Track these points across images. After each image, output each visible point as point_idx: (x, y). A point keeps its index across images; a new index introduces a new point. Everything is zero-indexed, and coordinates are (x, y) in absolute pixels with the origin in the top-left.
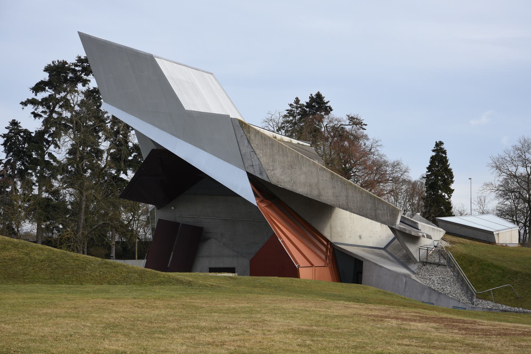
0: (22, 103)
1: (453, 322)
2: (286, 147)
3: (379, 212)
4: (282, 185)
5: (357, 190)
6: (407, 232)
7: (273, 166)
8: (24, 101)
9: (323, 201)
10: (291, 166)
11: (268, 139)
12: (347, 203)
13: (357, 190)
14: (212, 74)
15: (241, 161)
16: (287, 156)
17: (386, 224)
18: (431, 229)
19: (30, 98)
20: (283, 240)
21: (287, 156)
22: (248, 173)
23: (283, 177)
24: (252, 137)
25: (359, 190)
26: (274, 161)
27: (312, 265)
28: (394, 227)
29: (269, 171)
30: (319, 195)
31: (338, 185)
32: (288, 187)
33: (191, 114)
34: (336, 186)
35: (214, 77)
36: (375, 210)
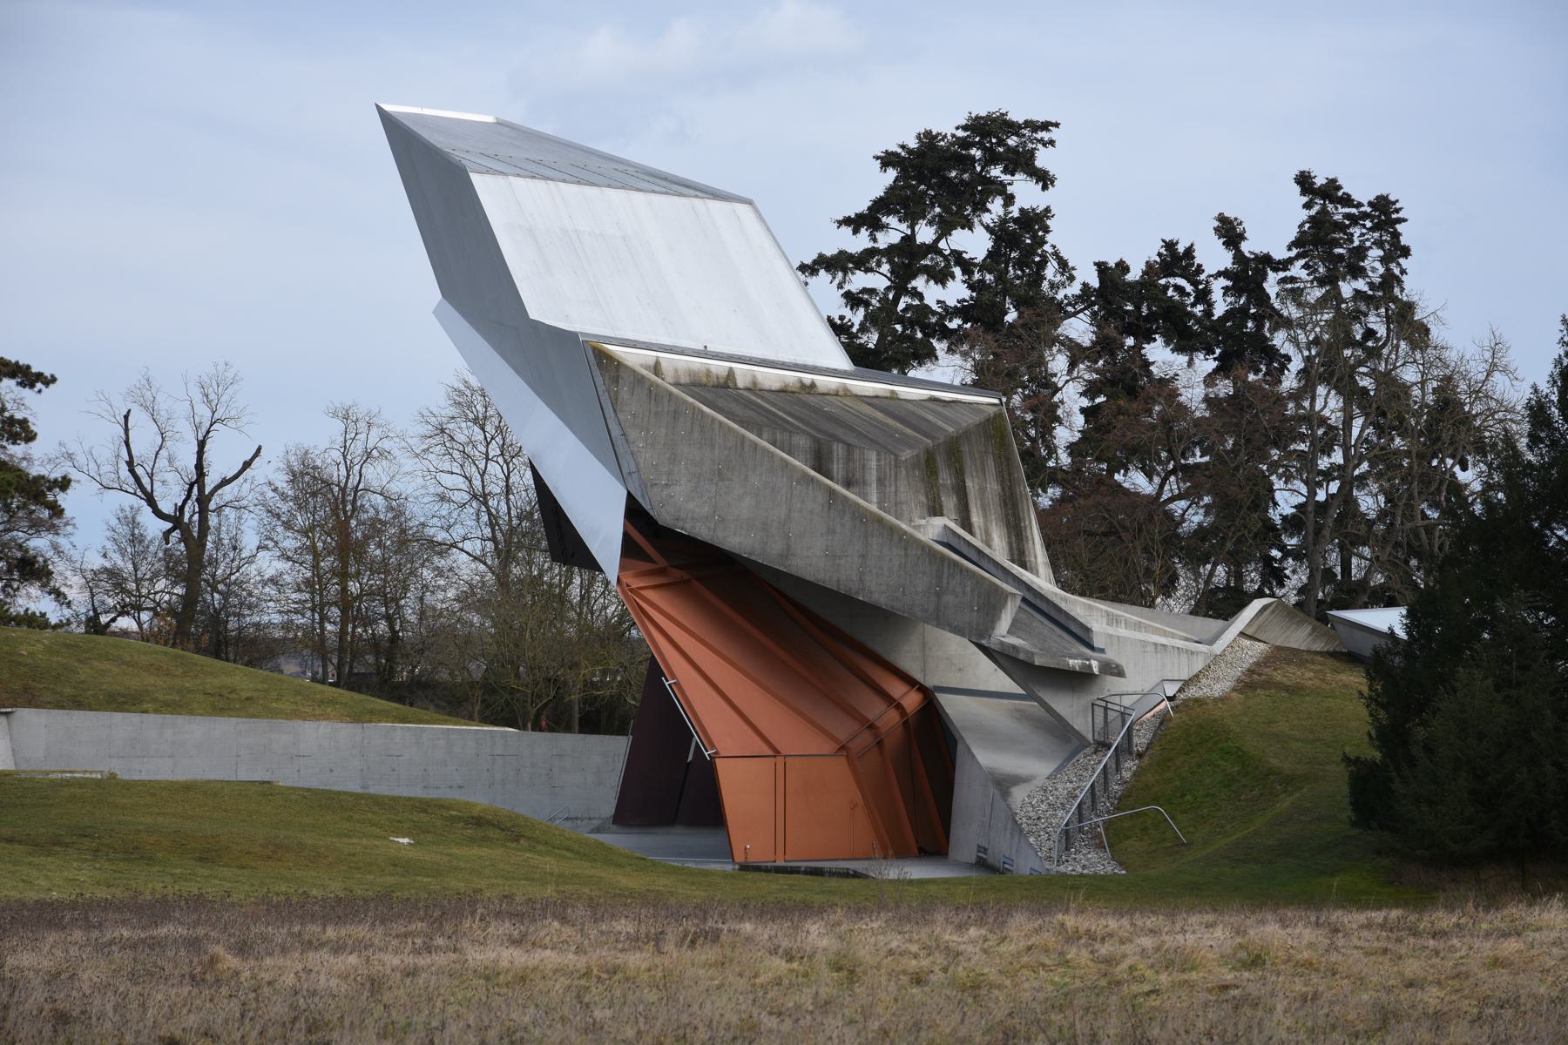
0: (803, 268)
1: (385, 898)
2: (713, 419)
3: (949, 599)
4: (688, 526)
5: (896, 538)
6: (1021, 656)
7: (670, 473)
8: (808, 261)
9: (793, 572)
10: (720, 473)
11: (666, 400)
12: (861, 576)
13: (896, 538)
14: (750, 202)
15: (615, 455)
16: (712, 447)
17: (963, 635)
18: (1150, 648)
19: (830, 251)
20: (683, 679)
21: (712, 447)
22: (629, 495)
23: (691, 505)
24: (624, 392)
25: (901, 539)
26: (673, 460)
27: (777, 753)
28: (984, 642)
29: (655, 489)
30: (786, 554)
31: (843, 525)
32: (702, 532)
33: (537, 325)
34: (838, 529)
35: (756, 211)
36: (939, 595)
